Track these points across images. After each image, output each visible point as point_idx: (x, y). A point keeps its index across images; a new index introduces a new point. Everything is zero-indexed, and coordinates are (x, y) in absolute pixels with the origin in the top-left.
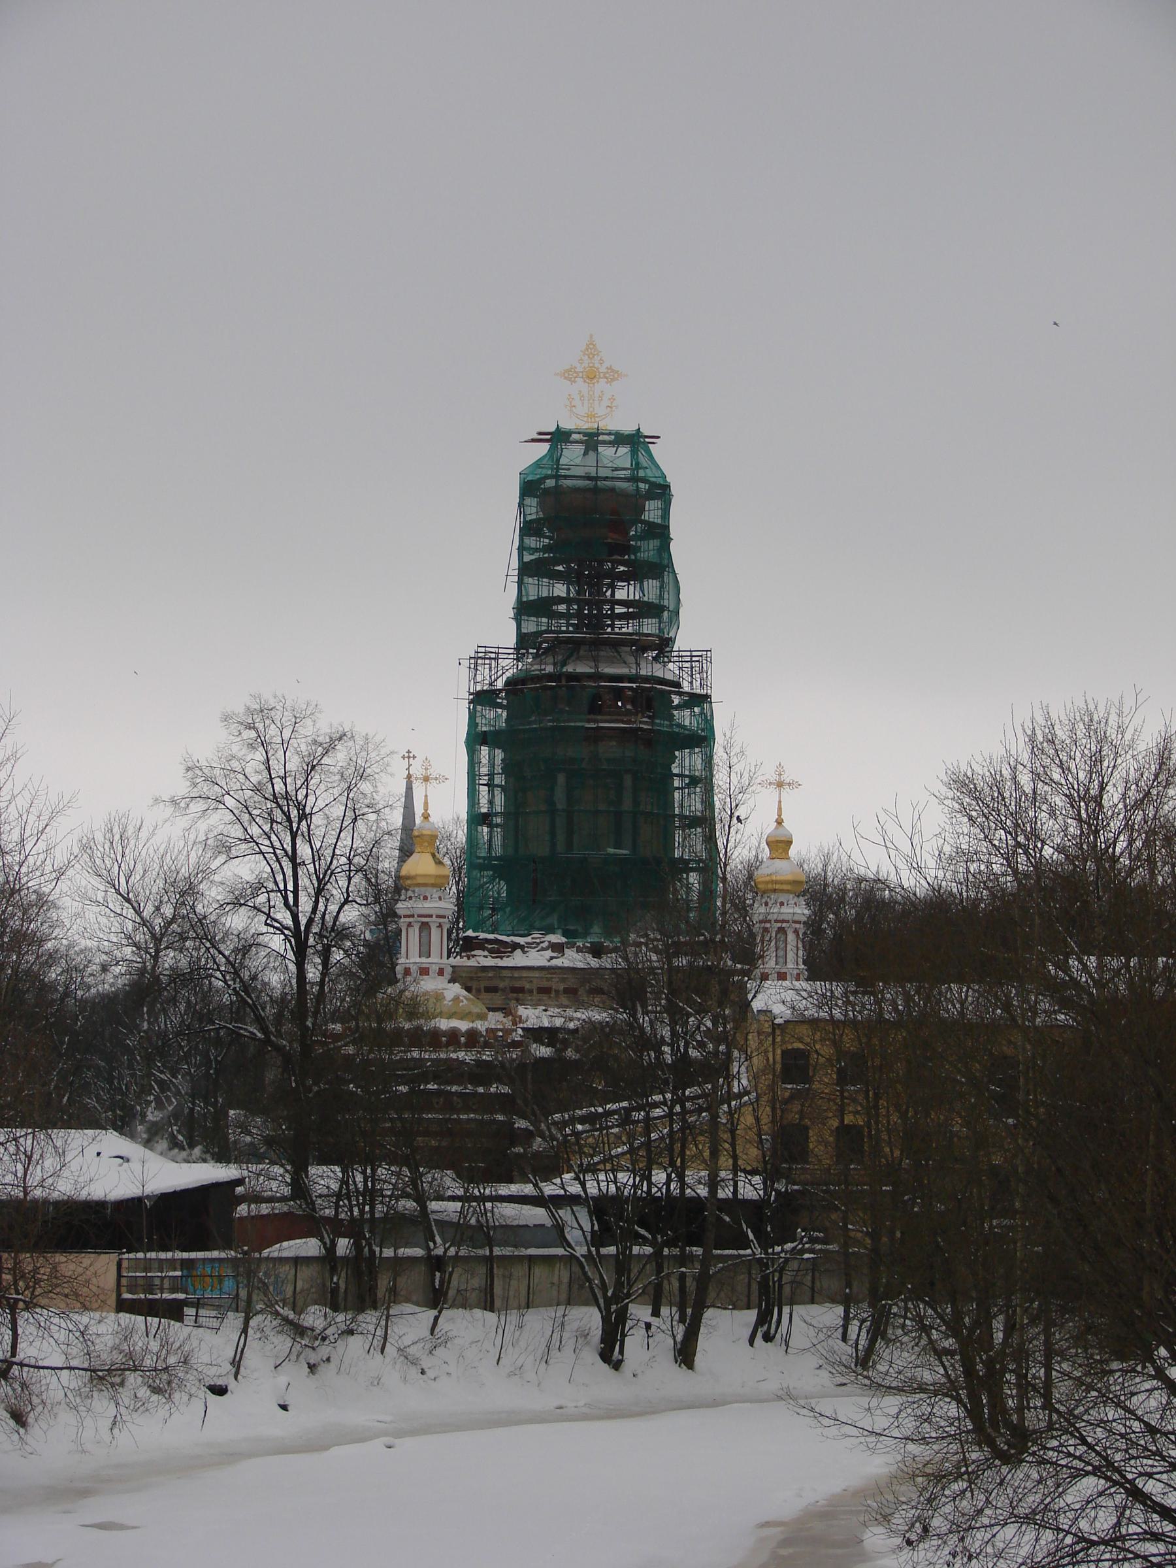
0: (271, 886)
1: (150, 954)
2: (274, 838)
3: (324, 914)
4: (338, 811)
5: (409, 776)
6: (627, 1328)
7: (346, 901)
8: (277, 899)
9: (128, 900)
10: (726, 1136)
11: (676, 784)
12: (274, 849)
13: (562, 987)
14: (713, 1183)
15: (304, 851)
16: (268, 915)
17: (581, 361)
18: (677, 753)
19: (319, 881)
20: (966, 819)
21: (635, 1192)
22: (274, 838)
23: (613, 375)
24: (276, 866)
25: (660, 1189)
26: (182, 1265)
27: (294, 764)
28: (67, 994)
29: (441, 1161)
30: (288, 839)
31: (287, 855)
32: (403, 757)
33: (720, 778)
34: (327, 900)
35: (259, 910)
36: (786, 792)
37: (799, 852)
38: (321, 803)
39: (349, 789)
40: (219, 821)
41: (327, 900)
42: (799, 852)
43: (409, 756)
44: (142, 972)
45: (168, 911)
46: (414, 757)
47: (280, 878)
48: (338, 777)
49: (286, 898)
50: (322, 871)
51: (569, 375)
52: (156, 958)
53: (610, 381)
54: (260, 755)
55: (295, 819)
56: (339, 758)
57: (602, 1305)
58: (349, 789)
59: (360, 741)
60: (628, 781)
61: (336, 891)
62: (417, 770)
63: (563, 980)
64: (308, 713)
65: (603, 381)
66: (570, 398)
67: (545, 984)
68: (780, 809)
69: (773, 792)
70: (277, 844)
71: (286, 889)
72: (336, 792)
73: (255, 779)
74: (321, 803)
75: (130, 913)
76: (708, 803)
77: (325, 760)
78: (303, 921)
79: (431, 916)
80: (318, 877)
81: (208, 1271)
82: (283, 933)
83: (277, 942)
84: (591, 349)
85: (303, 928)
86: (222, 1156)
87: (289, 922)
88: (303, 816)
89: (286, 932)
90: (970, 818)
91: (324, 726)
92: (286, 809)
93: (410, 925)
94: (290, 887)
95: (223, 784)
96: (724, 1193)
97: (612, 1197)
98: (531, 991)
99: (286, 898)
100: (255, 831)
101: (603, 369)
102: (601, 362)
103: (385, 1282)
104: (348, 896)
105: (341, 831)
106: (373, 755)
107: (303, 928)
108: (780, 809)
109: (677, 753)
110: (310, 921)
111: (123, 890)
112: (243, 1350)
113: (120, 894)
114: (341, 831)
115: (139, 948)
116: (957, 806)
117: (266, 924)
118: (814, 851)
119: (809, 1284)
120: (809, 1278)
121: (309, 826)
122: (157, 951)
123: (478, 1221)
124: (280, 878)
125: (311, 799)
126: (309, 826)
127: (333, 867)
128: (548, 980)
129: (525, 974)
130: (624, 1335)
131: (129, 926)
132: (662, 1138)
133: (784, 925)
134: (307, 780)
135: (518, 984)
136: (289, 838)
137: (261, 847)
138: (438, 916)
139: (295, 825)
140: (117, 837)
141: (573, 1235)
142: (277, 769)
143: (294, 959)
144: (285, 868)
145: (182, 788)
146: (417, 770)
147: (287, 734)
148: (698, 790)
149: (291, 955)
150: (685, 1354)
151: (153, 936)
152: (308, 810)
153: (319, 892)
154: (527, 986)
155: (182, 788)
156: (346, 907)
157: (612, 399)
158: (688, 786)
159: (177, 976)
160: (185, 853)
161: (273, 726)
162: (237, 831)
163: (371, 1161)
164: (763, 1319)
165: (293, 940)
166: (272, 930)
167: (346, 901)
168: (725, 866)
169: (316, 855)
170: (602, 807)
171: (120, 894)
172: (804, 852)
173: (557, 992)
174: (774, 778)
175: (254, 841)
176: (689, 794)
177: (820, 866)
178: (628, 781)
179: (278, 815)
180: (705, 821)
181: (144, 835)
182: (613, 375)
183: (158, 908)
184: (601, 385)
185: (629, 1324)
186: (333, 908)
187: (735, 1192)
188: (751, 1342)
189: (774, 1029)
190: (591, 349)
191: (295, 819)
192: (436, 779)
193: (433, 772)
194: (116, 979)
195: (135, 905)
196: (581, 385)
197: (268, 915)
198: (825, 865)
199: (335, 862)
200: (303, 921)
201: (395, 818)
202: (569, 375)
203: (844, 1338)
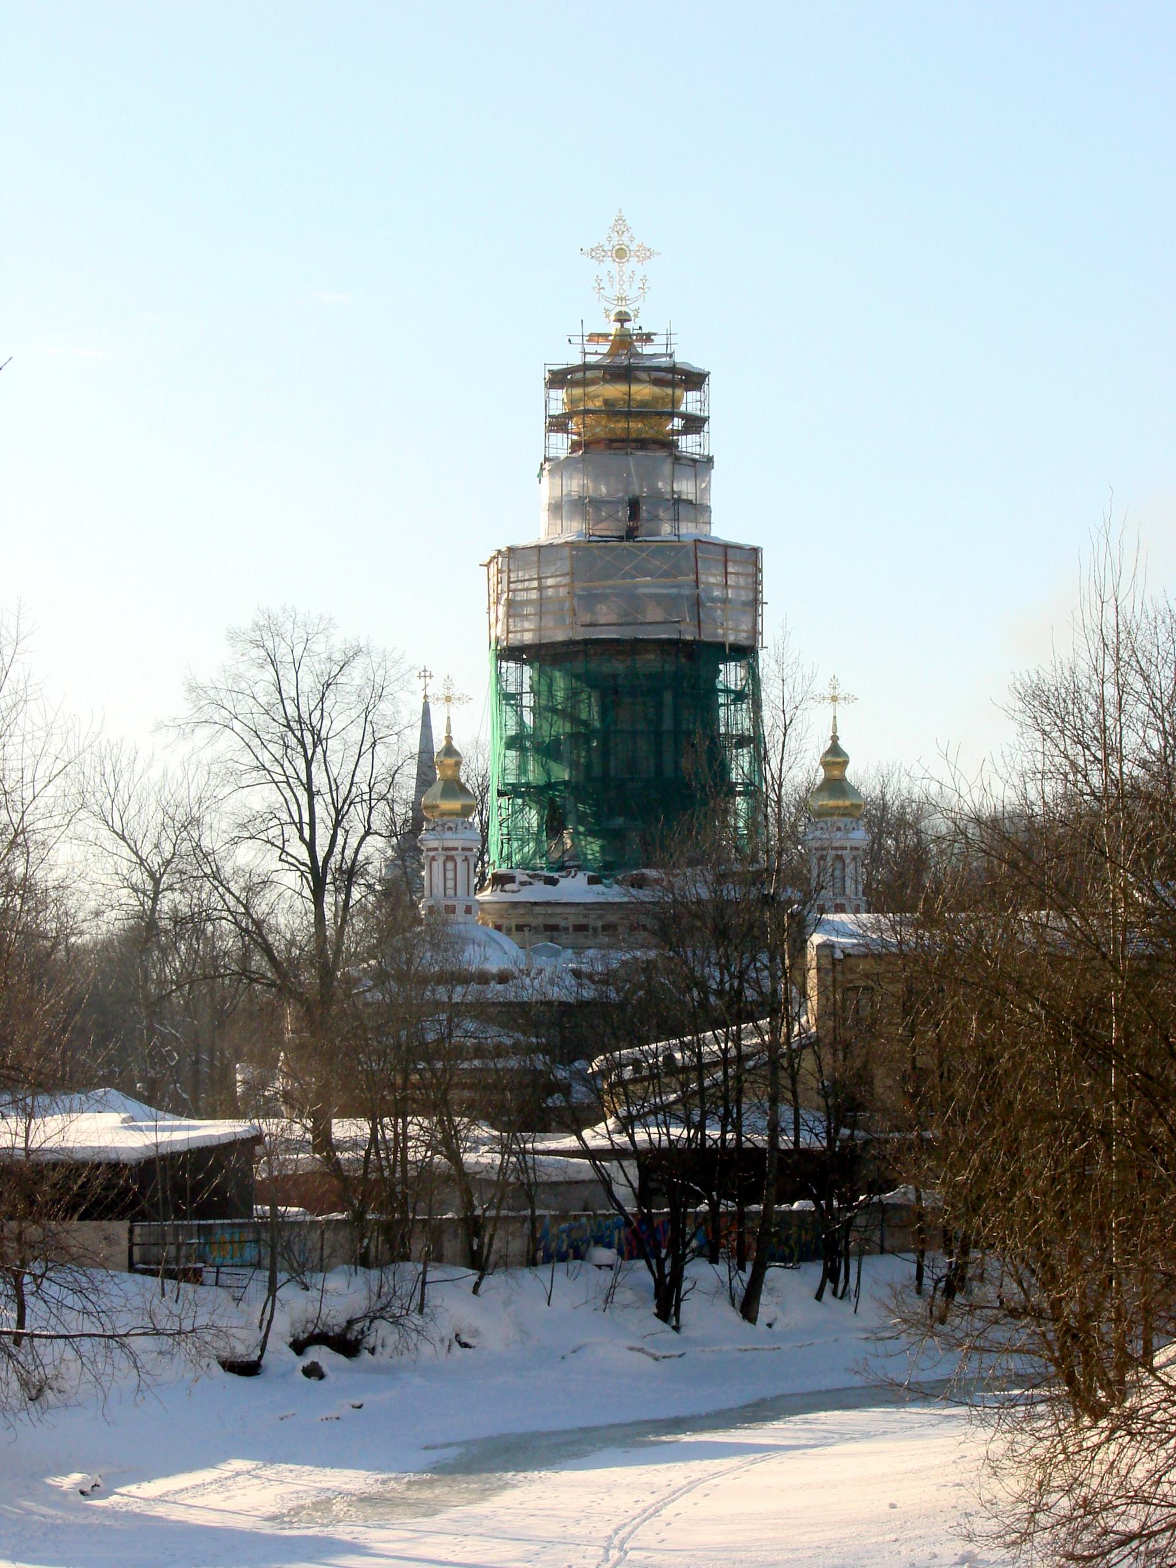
0: (285, 817)
1: (148, 896)
2: (286, 764)
3: (344, 848)
4: (355, 734)
5: (426, 696)
6: (682, 1293)
7: (368, 833)
8: (290, 831)
9: (123, 838)
10: (787, 1082)
11: (721, 700)
12: (287, 777)
13: (599, 924)
14: (774, 1130)
15: (320, 780)
16: (283, 850)
17: (609, 239)
18: (721, 667)
19: (338, 811)
20: (1038, 734)
21: (690, 1145)
22: (286, 764)
23: (646, 254)
24: (289, 795)
25: (715, 1141)
26: (198, 1230)
27: (308, 682)
28: (56, 942)
29: (477, 1113)
30: (301, 764)
31: (303, 784)
32: (419, 677)
33: (770, 693)
34: (347, 831)
35: (273, 844)
36: (842, 709)
37: (856, 773)
38: (337, 727)
39: (367, 711)
40: (228, 744)
41: (347, 831)
42: (856, 773)
43: (425, 675)
44: (140, 916)
45: (167, 848)
46: (431, 676)
47: (294, 808)
48: (354, 698)
49: (301, 831)
50: (341, 801)
51: (596, 253)
52: (155, 900)
53: (641, 261)
54: (269, 674)
55: (310, 747)
56: (356, 675)
57: (654, 1267)
58: (367, 711)
59: (377, 660)
60: (668, 697)
61: (356, 817)
62: (436, 688)
63: (600, 917)
64: (321, 627)
65: (634, 260)
66: (598, 280)
67: (582, 921)
68: (835, 725)
69: (826, 710)
70: (290, 771)
71: (301, 822)
72: (354, 714)
73: (263, 700)
74: (337, 727)
75: (126, 852)
76: (757, 721)
77: (340, 679)
78: (321, 854)
79: (456, 849)
80: (336, 809)
81: (227, 1237)
82: (299, 869)
83: (292, 879)
84: (620, 227)
85: (320, 864)
86: (235, 1113)
87: (305, 856)
88: (318, 741)
89: (303, 868)
90: (1044, 732)
91: (338, 643)
92: (298, 734)
93: (433, 859)
94: (306, 819)
95: (229, 705)
96: (785, 1141)
97: (664, 1149)
98: (566, 929)
99: (301, 831)
100: (266, 758)
101: (633, 247)
102: (632, 239)
103: (420, 1247)
104: (370, 828)
105: (359, 756)
106: (392, 672)
107: (320, 864)
108: (835, 725)
109: (721, 667)
110: (330, 853)
111: (118, 826)
112: (270, 1322)
113: (114, 831)
114: (359, 756)
115: (136, 890)
116: (1030, 721)
117: (281, 860)
118: (872, 771)
119: (878, 1241)
120: (878, 1233)
121: (325, 752)
122: (157, 893)
123: (518, 1179)
124: (294, 808)
125: (327, 722)
126: (325, 752)
127: (352, 796)
128: (585, 916)
129: (559, 910)
130: (679, 1301)
131: (124, 867)
132: (715, 1084)
133: (840, 852)
134: (322, 699)
135: (552, 921)
136: (304, 765)
137: (274, 775)
138: (463, 849)
139: (310, 753)
140: (108, 770)
141: (622, 1192)
142: (289, 690)
143: (311, 897)
144: (298, 794)
145: (185, 711)
146: (436, 688)
147: (298, 651)
148: (744, 706)
149: (307, 893)
150: (748, 1308)
151: (152, 875)
152: (323, 734)
153: (337, 824)
154: (563, 923)
155: (185, 711)
156: (368, 838)
157: (644, 280)
158: (734, 702)
159: (178, 920)
160: (185, 785)
161: (283, 644)
162: (248, 759)
163: (400, 1112)
164: (831, 1274)
165: (309, 876)
166: (286, 866)
167: (368, 833)
168: (780, 786)
169: (334, 785)
170: (641, 726)
171: (114, 831)
172: (861, 773)
173: (595, 929)
174: (828, 692)
175: (265, 769)
176: (736, 711)
177: (878, 788)
178: (668, 697)
179: (293, 742)
180: (754, 741)
181: (138, 768)
182: (646, 254)
183: (156, 846)
184: (632, 265)
185: (686, 1286)
186: (353, 841)
187: (796, 1143)
188: (819, 1297)
189: (834, 965)
190: (620, 227)
191: (310, 747)
192: (459, 699)
193: (455, 692)
194: (113, 923)
195: (132, 845)
196: (610, 264)
197: (283, 850)
198: (884, 786)
199: (354, 789)
200: (321, 854)
201: (413, 741)
202: (596, 253)
203: (919, 1291)
